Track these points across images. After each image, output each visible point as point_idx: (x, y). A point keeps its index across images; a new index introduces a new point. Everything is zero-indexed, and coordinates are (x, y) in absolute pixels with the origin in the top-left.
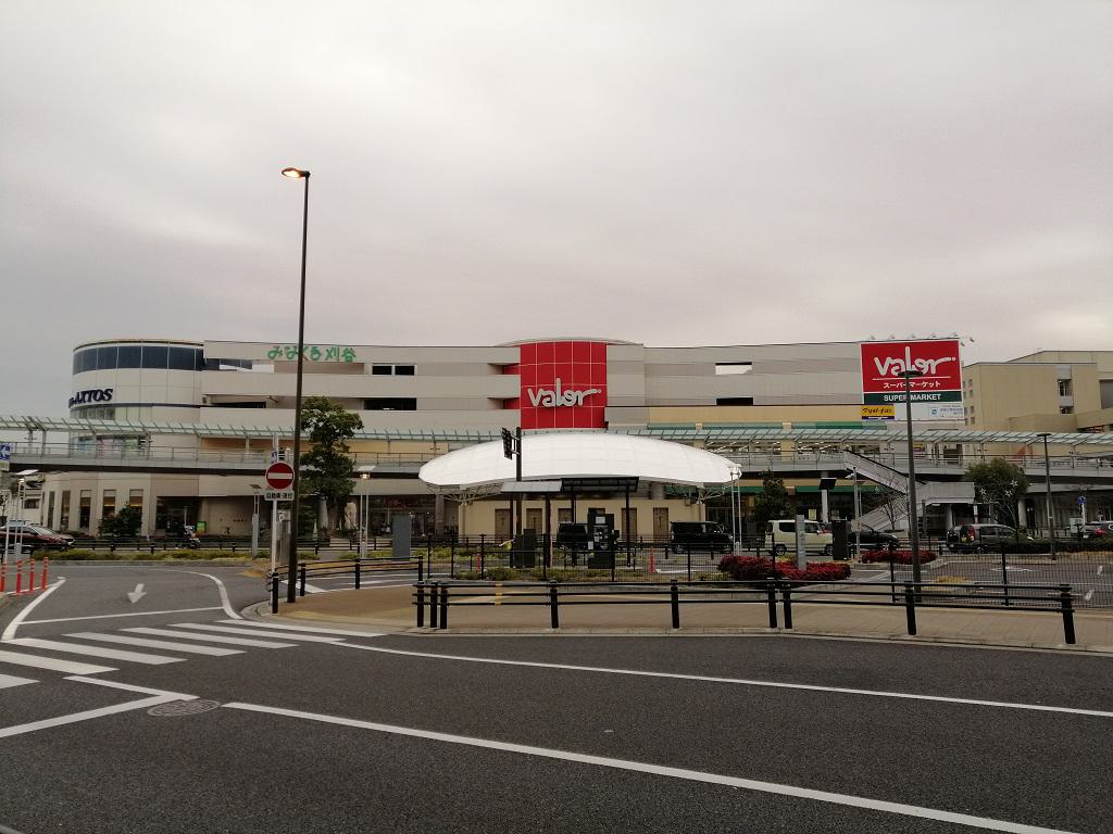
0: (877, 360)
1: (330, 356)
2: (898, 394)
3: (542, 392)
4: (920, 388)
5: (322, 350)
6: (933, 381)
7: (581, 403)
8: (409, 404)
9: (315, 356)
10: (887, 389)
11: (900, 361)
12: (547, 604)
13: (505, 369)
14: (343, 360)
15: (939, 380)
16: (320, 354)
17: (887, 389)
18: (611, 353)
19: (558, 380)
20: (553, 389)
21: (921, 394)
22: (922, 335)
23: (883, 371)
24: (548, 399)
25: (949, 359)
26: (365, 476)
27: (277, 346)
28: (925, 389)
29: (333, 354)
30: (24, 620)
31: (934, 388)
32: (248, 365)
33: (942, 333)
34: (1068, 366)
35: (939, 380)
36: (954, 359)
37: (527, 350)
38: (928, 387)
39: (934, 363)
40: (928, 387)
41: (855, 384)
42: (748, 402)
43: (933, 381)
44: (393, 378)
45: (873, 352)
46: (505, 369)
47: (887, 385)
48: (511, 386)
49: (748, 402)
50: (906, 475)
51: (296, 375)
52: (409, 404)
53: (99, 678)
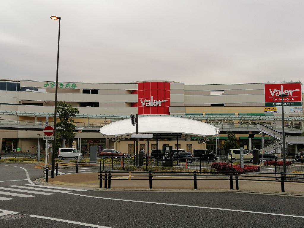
0: (270, 90)
1: (67, 86)
2: (278, 103)
3: (146, 101)
5: (63, 84)
6: (291, 98)
7: (160, 105)
8: (96, 105)
9: (61, 86)
10: (274, 101)
11: (149, 101)
12: (148, 179)
13: (132, 92)
14: (72, 88)
16: (63, 86)
17: (274, 101)
18: (172, 87)
19: (152, 97)
20: (150, 99)
21: (286, 103)
22: (288, 81)
23: (273, 94)
24: (148, 103)
27: (47, 82)
29: (68, 86)
31: (292, 101)
33: (295, 80)
36: (299, 90)
37: (140, 85)
38: (289, 101)
39: (291, 92)
40: (289, 101)
41: (262, 99)
42: (222, 105)
43: (291, 98)
44: (90, 95)
45: (269, 87)
46: (132, 92)
47: (274, 100)
48: (134, 98)
49: (222, 105)
51: (55, 94)
52: (96, 105)
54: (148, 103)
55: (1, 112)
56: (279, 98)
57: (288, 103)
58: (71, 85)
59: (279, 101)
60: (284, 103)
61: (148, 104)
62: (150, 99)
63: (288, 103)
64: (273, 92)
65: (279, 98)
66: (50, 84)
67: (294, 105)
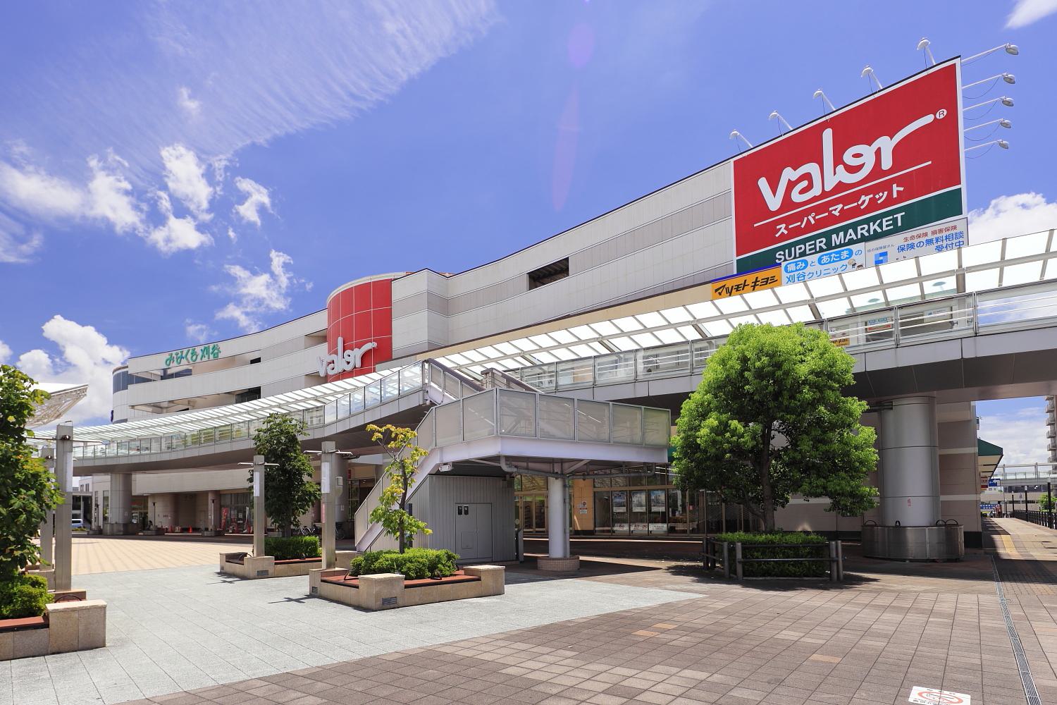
0: (763, 184)
4: (857, 212)
6: (887, 186)
10: (783, 237)
11: (811, 168)
15: (898, 181)
17: (783, 237)
20: (336, 353)
21: (854, 226)
23: (774, 203)
24: (805, 184)
25: (929, 119)
26: (907, 562)
28: (867, 211)
30: (774, 193)
32: (54, 515)
34: (591, 362)
35: (898, 181)
38: (873, 205)
39: (886, 144)
40: (873, 205)
47: (782, 228)
50: (960, 266)
53: (926, 562)
54: (805, 184)
55: (1054, 609)
56: (807, 212)
57: (867, 221)
58: (211, 351)
59: (810, 228)
60: (785, 253)
61: (802, 192)
62: (336, 353)
63: (867, 221)
64: (774, 193)
65: (807, 212)
66: (175, 357)
67: (909, 224)
